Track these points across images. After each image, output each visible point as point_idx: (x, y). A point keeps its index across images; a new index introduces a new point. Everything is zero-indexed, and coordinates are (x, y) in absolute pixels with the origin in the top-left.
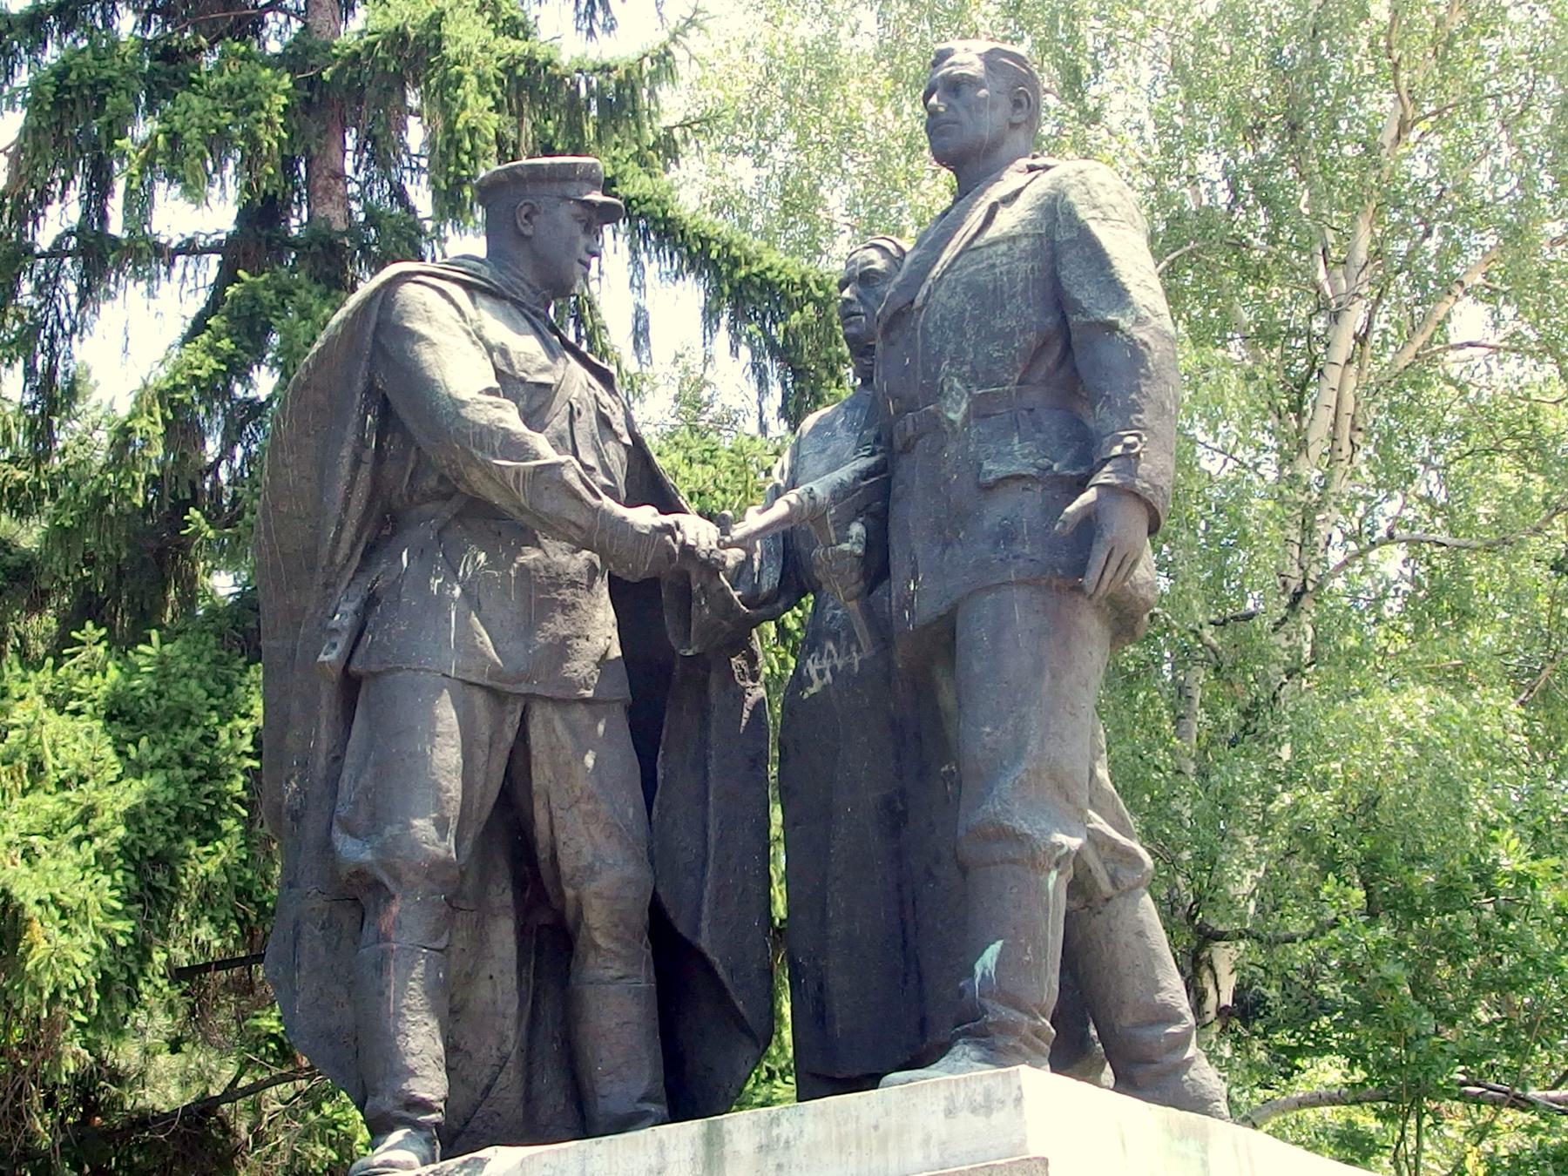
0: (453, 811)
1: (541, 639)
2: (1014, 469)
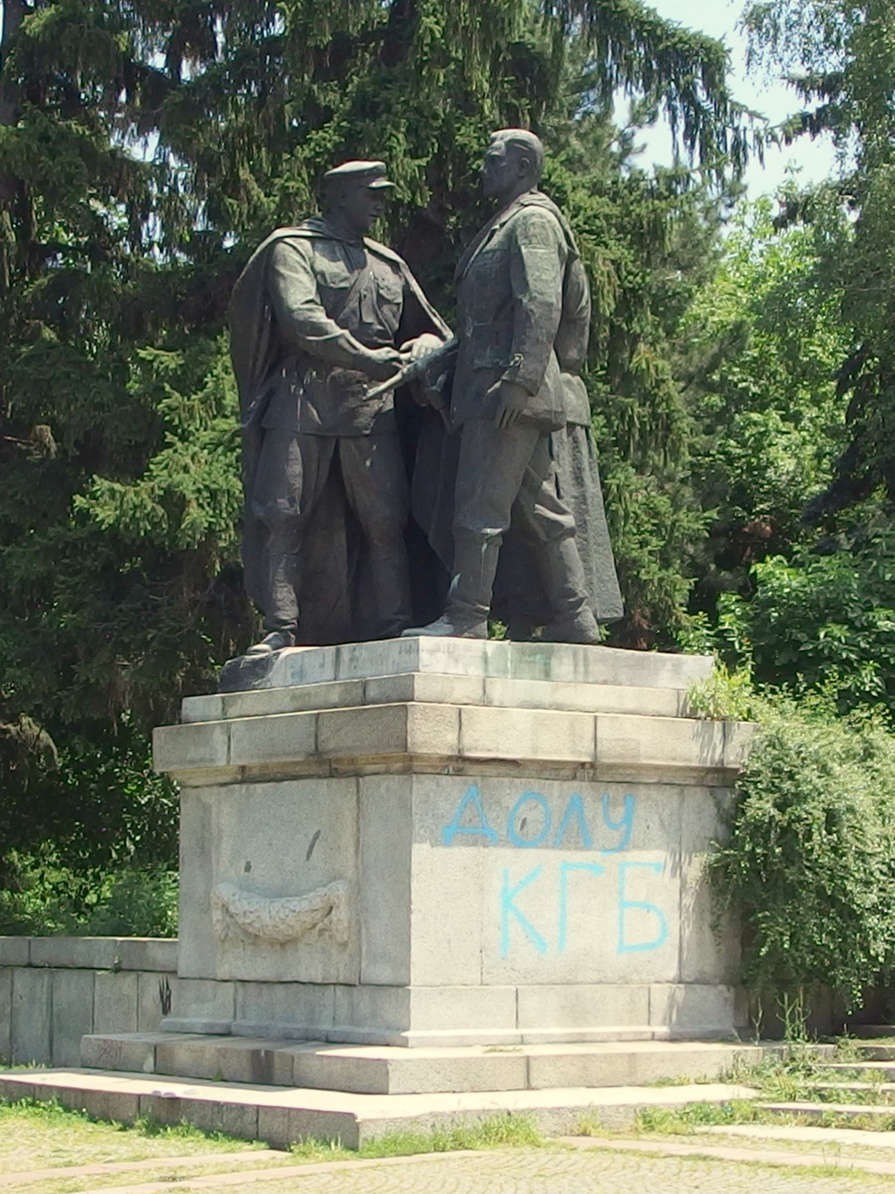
0: (298, 495)
1: (341, 410)
2: (484, 364)
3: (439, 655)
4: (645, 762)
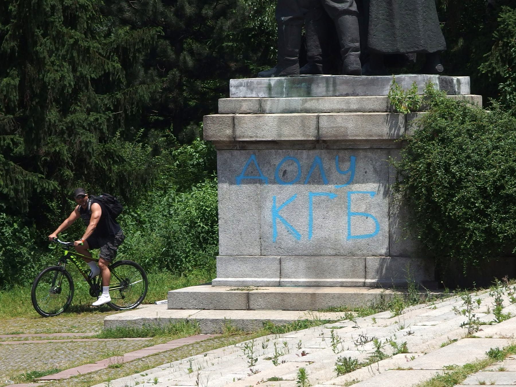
3: (241, 88)
4: (351, 138)
